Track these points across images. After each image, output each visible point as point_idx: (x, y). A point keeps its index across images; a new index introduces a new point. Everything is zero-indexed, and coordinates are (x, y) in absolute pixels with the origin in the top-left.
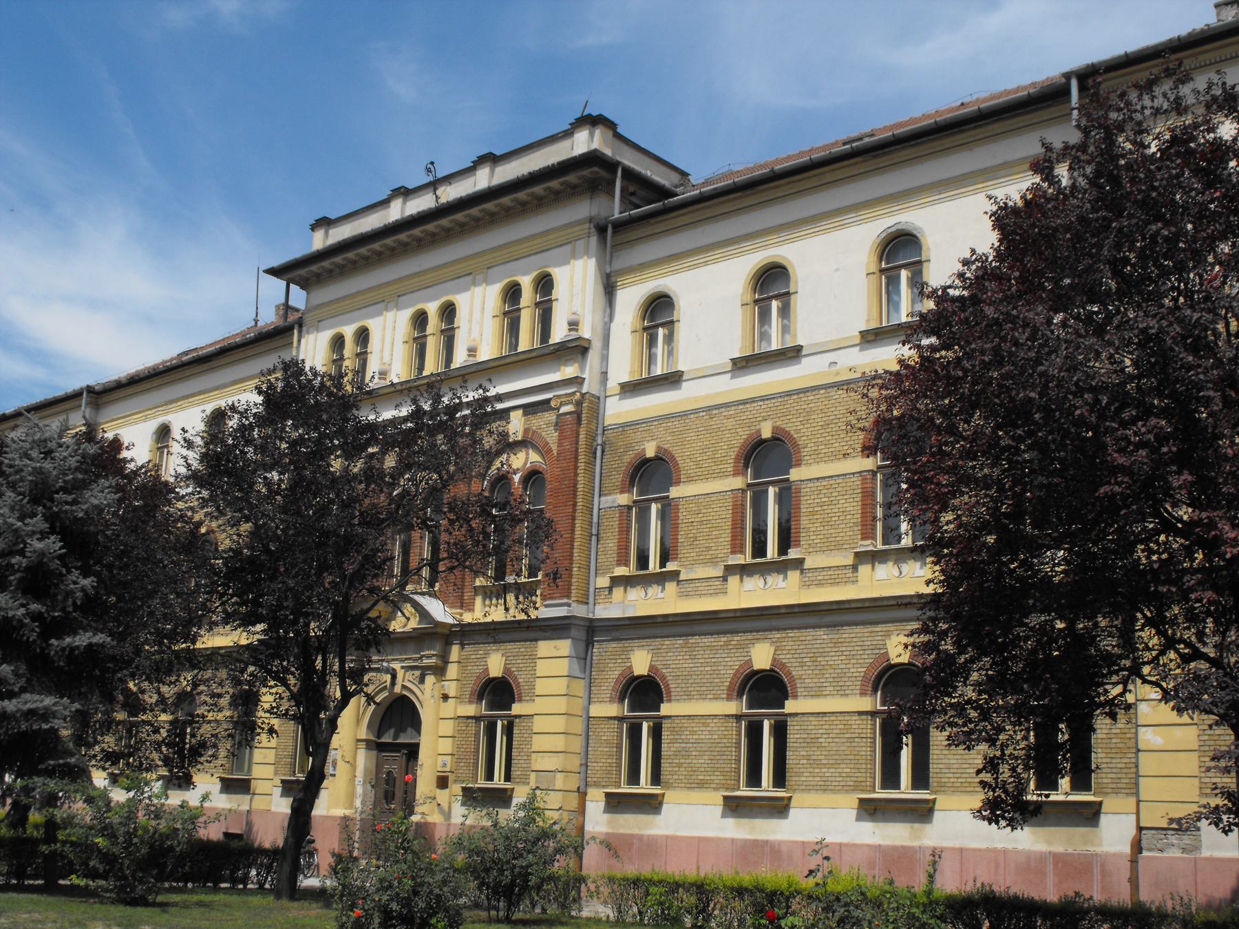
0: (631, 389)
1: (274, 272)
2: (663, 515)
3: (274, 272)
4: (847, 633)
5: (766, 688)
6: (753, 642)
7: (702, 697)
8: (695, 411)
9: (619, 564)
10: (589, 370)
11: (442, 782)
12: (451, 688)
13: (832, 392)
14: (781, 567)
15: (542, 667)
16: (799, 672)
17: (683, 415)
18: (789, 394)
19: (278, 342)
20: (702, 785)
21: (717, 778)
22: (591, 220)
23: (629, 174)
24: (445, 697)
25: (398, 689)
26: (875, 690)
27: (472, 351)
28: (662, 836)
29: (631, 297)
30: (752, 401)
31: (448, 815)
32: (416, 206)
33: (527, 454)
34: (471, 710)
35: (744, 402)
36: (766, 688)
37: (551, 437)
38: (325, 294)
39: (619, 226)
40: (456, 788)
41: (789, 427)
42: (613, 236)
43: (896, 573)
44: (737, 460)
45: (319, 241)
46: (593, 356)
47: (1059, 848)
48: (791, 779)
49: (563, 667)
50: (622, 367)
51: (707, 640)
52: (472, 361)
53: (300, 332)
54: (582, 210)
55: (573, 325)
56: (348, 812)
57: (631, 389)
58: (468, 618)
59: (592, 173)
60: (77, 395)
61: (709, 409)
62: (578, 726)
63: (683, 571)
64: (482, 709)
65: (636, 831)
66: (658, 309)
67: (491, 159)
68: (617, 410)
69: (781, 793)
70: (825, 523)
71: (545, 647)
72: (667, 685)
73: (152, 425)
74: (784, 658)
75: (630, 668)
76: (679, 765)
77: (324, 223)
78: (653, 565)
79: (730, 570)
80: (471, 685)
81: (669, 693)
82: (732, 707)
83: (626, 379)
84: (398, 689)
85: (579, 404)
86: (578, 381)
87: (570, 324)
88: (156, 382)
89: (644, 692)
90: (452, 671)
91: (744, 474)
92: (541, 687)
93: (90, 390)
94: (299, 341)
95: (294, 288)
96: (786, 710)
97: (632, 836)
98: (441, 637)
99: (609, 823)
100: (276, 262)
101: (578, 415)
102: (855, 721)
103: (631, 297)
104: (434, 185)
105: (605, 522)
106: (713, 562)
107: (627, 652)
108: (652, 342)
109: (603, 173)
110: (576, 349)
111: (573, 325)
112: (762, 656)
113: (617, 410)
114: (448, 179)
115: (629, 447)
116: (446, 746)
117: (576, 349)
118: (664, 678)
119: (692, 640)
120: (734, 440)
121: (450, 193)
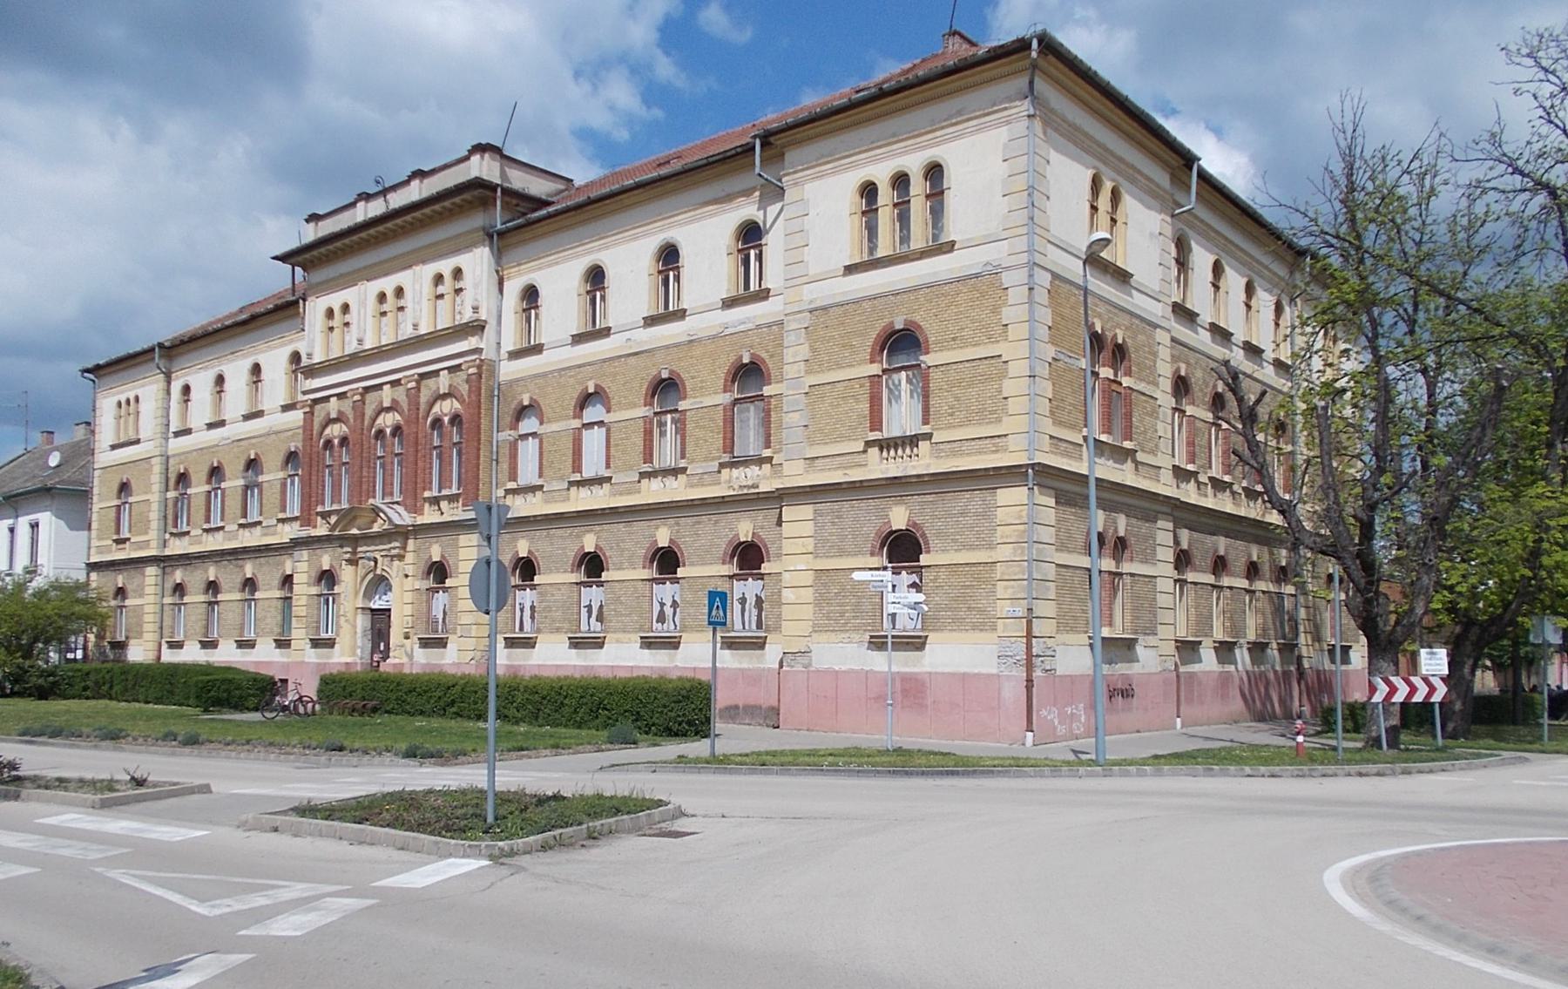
0: (515, 355)
1: (283, 258)
3: (283, 258)
6: (738, 520)
10: (484, 342)
12: (410, 570)
13: (632, 360)
15: (463, 553)
17: (544, 375)
18: (604, 361)
19: (291, 311)
20: (558, 630)
21: (566, 625)
22: (484, 229)
23: (508, 192)
25: (379, 572)
26: (652, 562)
29: (514, 287)
31: (411, 657)
32: (376, 208)
35: (579, 366)
37: (464, 389)
38: (319, 275)
39: (501, 234)
40: (415, 639)
41: (917, 318)
42: (502, 242)
44: (875, 343)
45: (311, 233)
46: (490, 330)
47: (745, 666)
49: (809, 528)
50: (510, 342)
51: (559, 532)
52: (361, 348)
54: (477, 220)
55: (476, 309)
56: (349, 660)
57: (515, 355)
58: (420, 520)
59: (478, 193)
60: (152, 350)
62: (158, 607)
66: (531, 295)
67: (420, 174)
72: (923, 535)
73: (247, 364)
77: (314, 218)
79: (643, 475)
80: (423, 566)
81: (927, 543)
83: (511, 348)
84: (379, 572)
85: (479, 367)
86: (478, 351)
88: (209, 340)
89: (179, 589)
90: (410, 558)
91: (651, 404)
92: (788, 546)
93: (161, 345)
95: (298, 269)
96: (922, 563)
98: (402, 534)
100: (278, 253)
101: (479, 375)
103: (514, 287)
104: (384, 192)
105: (501, 451)
106: (562, 478)
107: (515, 540)
108: (528, 320)
109: (488, 193)
110: (477, 327)
111: (476, 309)
112: (899, 518)
114: (394, 188)
117: (477, 327)
118: (762, 541)
120: (725, 364)
121: (398, 200)
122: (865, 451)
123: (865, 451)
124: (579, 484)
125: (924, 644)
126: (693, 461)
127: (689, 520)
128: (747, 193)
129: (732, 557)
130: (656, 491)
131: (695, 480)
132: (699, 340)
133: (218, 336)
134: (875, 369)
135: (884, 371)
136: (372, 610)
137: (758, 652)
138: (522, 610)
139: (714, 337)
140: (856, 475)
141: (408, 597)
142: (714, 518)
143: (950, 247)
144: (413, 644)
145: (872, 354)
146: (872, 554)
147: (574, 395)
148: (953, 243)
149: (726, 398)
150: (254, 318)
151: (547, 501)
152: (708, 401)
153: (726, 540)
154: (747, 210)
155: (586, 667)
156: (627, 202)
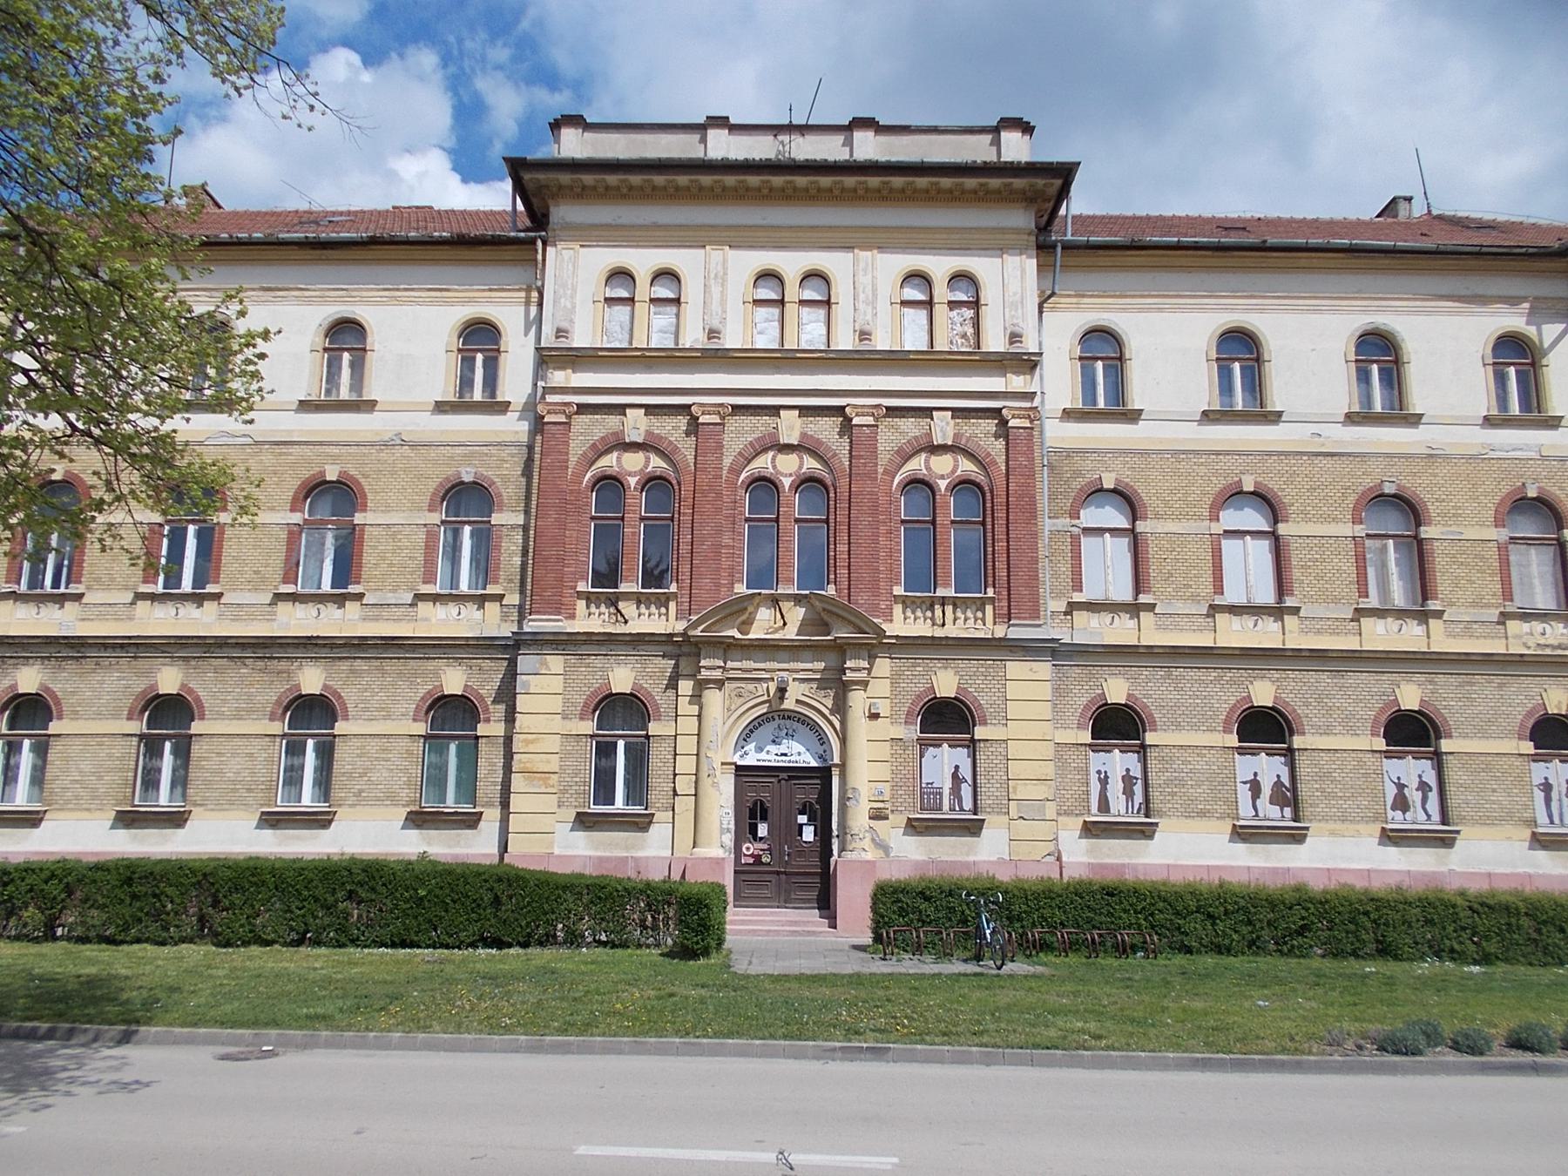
2: (199, 535)
4: (1351, 679)
5: (312, 712)
7: (1195, 728)
8: (1160, 452)
9: (285, 581)
11: (878, 815)
14: (198, 599)
16: (350, 695)
24: (874, 716)
27: (560, 333)
28: (1161, 865)
30: (1227, 453)
33: (801, 459)
34: (900, 731)
36: (312, 712)
43: (315, 613)
48: (336, 793)
53: (545, 244)
57: (1068, 415)
61: (1176, 452)
63: (1448, 611)
64: (139, 726)
65: (1127, 861)
68: (1058, 434)
69: (638, 809)
70: (1319, 578)
71: (1015, 668)
74: (1288, 698)
75: (298, 687)
76: (1173, 794)
78: (187, 585)
79: (279, 597)
82: (278, 728)
87: (559, 330)
94: (544, 251)
97: (1123, 865)
99: (1090, 852)
102: (406, 742)
106: (1195, 598)
107: (149, 672)
113: (1058, 434)
114: (804, 129)
115: (1078, 473)
116: (884, 772)
119: (1176, 673)
122: (133, 603)
123: (133, 603)
124: (294, 598)
125: (330, 822)
126: (1452, 604)
127: (1452, 679)
128: (1513, 301)
129: (286, 709)
130: (297, 621)
131: (1458, 629)
132: (1446, 457)
133: (255, 253)
134: (297, 518)
135: (443, 522)
136: (739, 768)
137: (1442, 851)
138: (1104, 782)
139: (1472, 457)
140: (1496, 647)
141: (885, 751)
142: (1497, 680)
143: (370, 406)
144: (893, 832)
145: (295, 499)
146: (129, 718)
147: (1218, 484)
148: (1280, 414)
149: (1503, 534)
150: (374, 241)
151: (1451, 635)
152: (1172, 527)
153: (1523, 710)
154: (1514, 320)
155: (1275, 871)
156: (1303, 263)
